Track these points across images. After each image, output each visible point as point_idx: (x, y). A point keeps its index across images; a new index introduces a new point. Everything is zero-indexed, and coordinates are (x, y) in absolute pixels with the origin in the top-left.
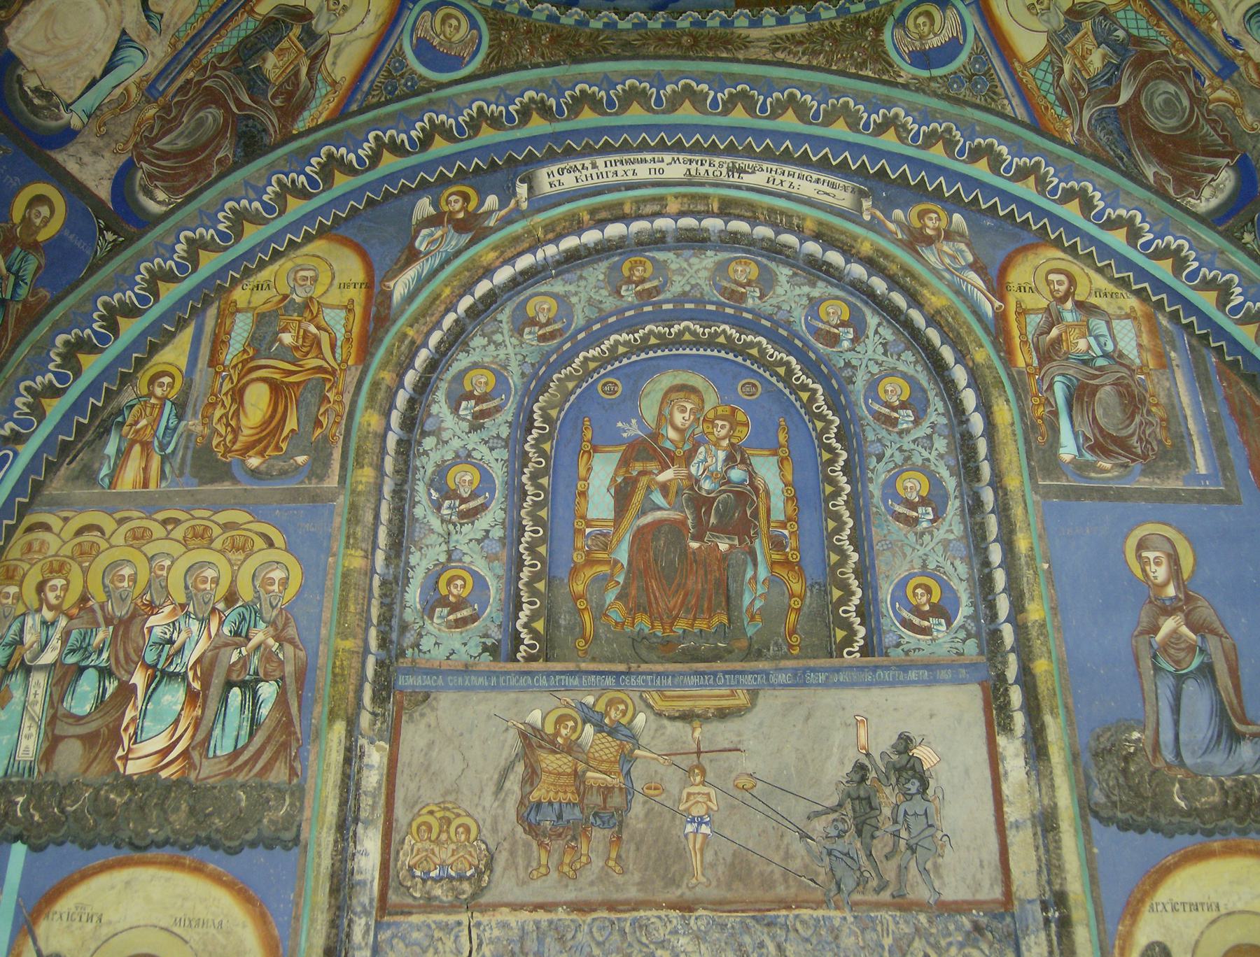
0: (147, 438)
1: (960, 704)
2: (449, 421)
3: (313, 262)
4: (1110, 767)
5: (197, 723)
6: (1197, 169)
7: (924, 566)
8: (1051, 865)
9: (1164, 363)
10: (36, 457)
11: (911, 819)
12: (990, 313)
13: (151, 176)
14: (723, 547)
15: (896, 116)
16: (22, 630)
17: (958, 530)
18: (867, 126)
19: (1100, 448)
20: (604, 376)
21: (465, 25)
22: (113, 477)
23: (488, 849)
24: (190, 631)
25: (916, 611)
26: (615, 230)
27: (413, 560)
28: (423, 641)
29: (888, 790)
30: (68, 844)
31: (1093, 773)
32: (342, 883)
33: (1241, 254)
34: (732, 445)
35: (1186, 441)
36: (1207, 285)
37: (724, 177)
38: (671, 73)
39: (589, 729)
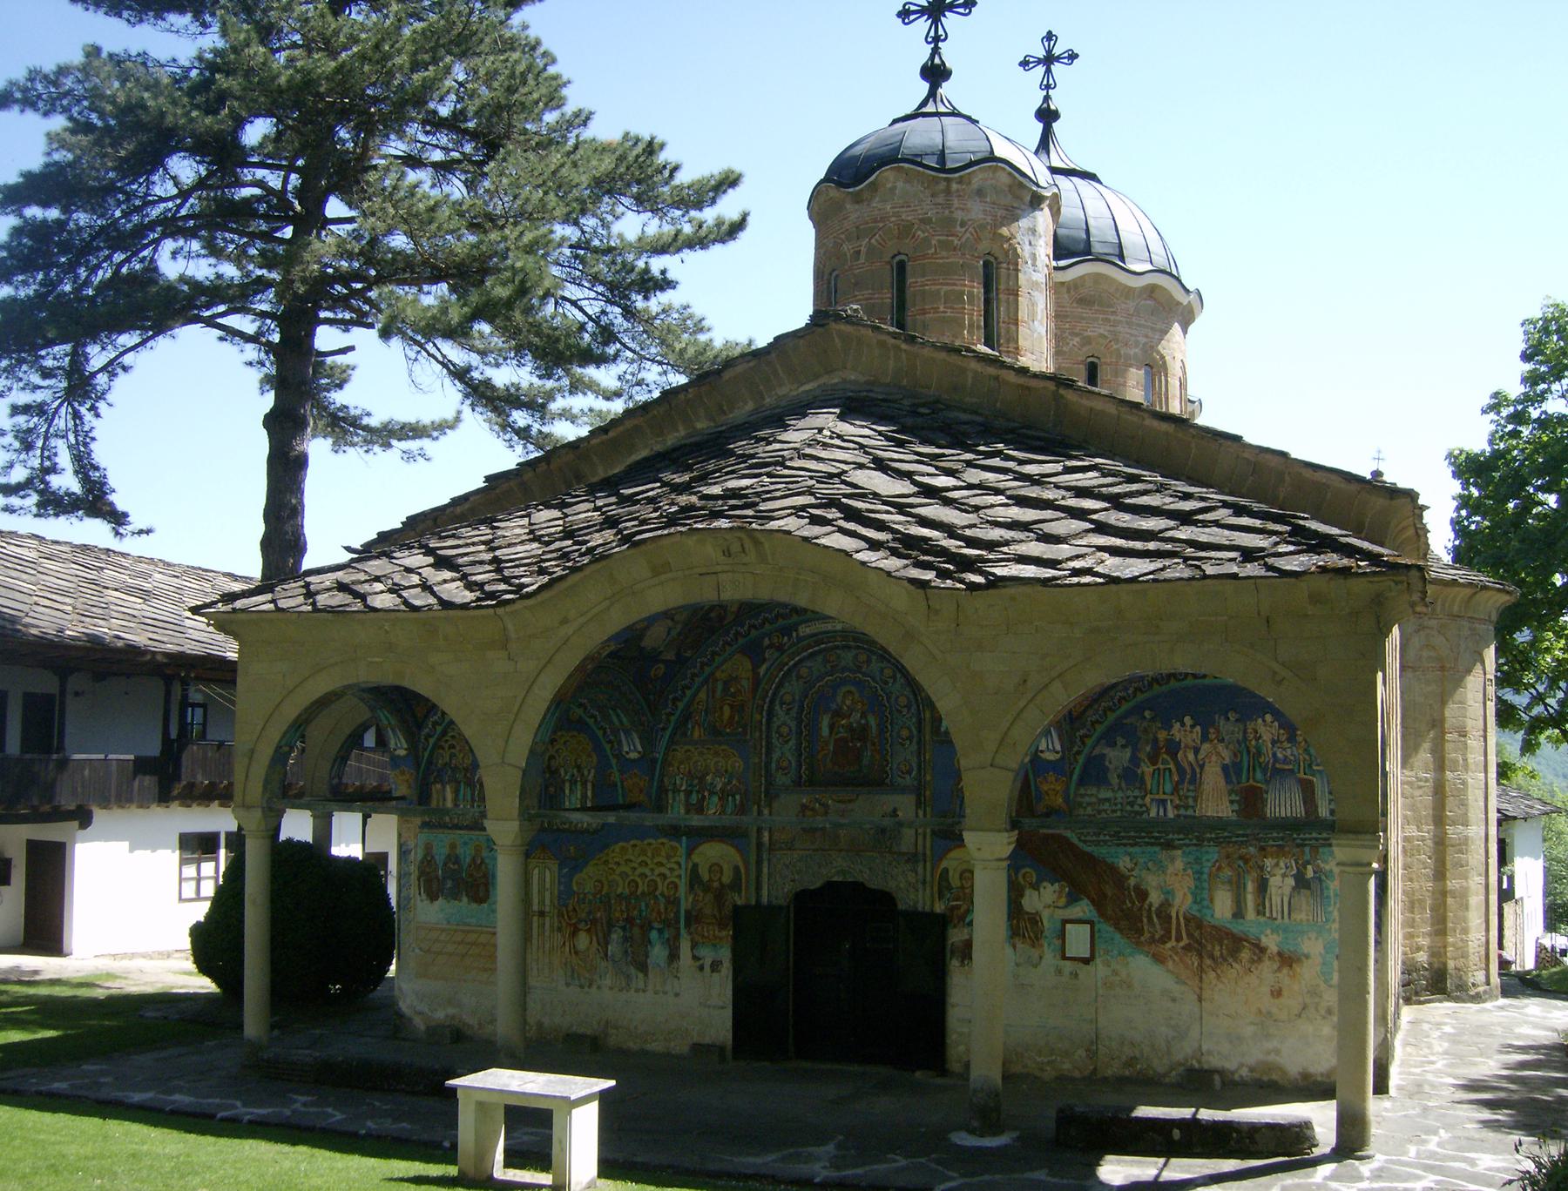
32: (759, 845)
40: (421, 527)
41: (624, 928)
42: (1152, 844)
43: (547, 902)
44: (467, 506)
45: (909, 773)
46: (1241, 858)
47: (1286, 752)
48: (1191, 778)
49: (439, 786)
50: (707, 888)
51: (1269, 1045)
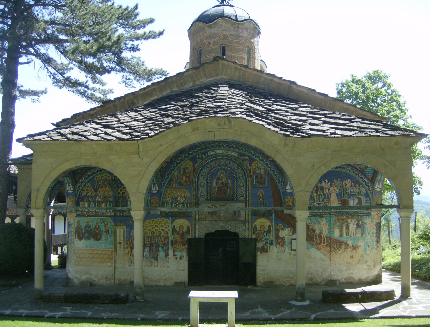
8: (248, 218)
9: (265, 174)
19: (257, 183)
32: (195, 219)
40: (78, 118)
41: (150, 247)
42: (316, 216)
43: (122, 239)
44: (95, 111)
45: (243, 196)
46: (342, 219)
47: (354, 189)
48: (328, 197)
49: (82, 203)
50: (178, 233)
51: (349, 272)
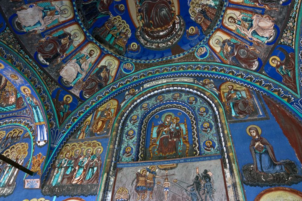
0: (84, 131)
1: (217, 163)
2: (129, 124)
3: (110, 103)
4: (247, 173)
5: (84, 174)
6: (251, 63)
7: (209, 139)
9: (251, 97)
10: (67, 134)
11: (207, 187)
12: (218, 94)
13: (85, 93)
14: (175, 140)
15: (199, 66)
16: (62, 161)
17: (215, 132)
18: (194, 68)
20: (156, 115)
21: (131, 65)
22: (78, 137)
23: (129, 195)
24: (85, 160)
25: (208, 147)
26: (156, 92)
27: (122, 146)
28: (122, 159)
29: (203, 181)
30: (62, 196)
31: (243, 175)
33: (263, 76)
34: (177, 123)
35: (257, 110)
36: (257, 82)
37: (173, 81)
38: (163, 67)
39: (148, 172)
45: (213, 146)
